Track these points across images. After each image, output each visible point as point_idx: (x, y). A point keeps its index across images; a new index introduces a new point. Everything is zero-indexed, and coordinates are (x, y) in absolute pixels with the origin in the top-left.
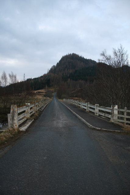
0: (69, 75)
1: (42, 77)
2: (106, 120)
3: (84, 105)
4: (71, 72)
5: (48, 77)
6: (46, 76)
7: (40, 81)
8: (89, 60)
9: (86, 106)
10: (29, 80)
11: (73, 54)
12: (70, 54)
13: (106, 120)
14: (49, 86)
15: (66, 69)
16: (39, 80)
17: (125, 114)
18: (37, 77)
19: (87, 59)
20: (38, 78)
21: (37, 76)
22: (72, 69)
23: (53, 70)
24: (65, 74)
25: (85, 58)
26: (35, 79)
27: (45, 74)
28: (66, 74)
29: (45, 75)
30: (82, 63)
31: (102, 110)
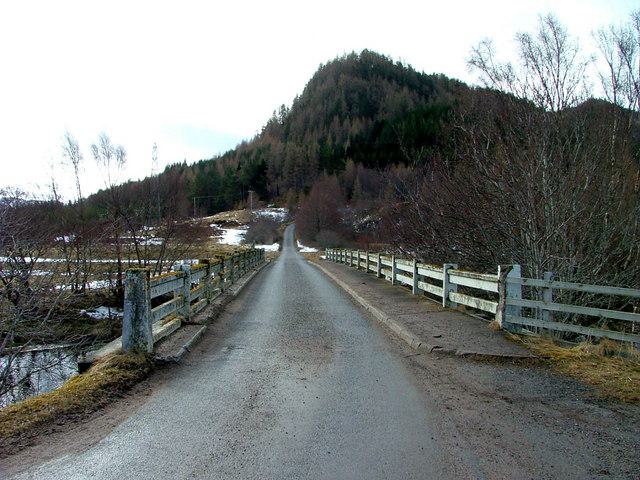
0: (347, 145)
1: (230, 155)
2: (169, 324)
3: (404, 269)
4: (356, 131)
5: (257, 158)
6: (251, 152)
7: (222, 174)
8: (434, 77)
9: (438, 283)
10: (175, 172)
11: (365, 53)
12: (353, 55)
13: (169, 324)
14: (267, 198)
15: (336, 118)
16: (220, 167)
17: (548, 295)
18: (208, 156)
19: (425, 75)
20: (213, 162)
21: (208, 154)
22: (360, 118)
23: (280, 130)
24: (329, 143)
25: (418, 69)
26: (202, 165)
27: (244, 144)
28: (334, 139)
29: (243, 152)
30: (406, 90)
31: (432, 279)
